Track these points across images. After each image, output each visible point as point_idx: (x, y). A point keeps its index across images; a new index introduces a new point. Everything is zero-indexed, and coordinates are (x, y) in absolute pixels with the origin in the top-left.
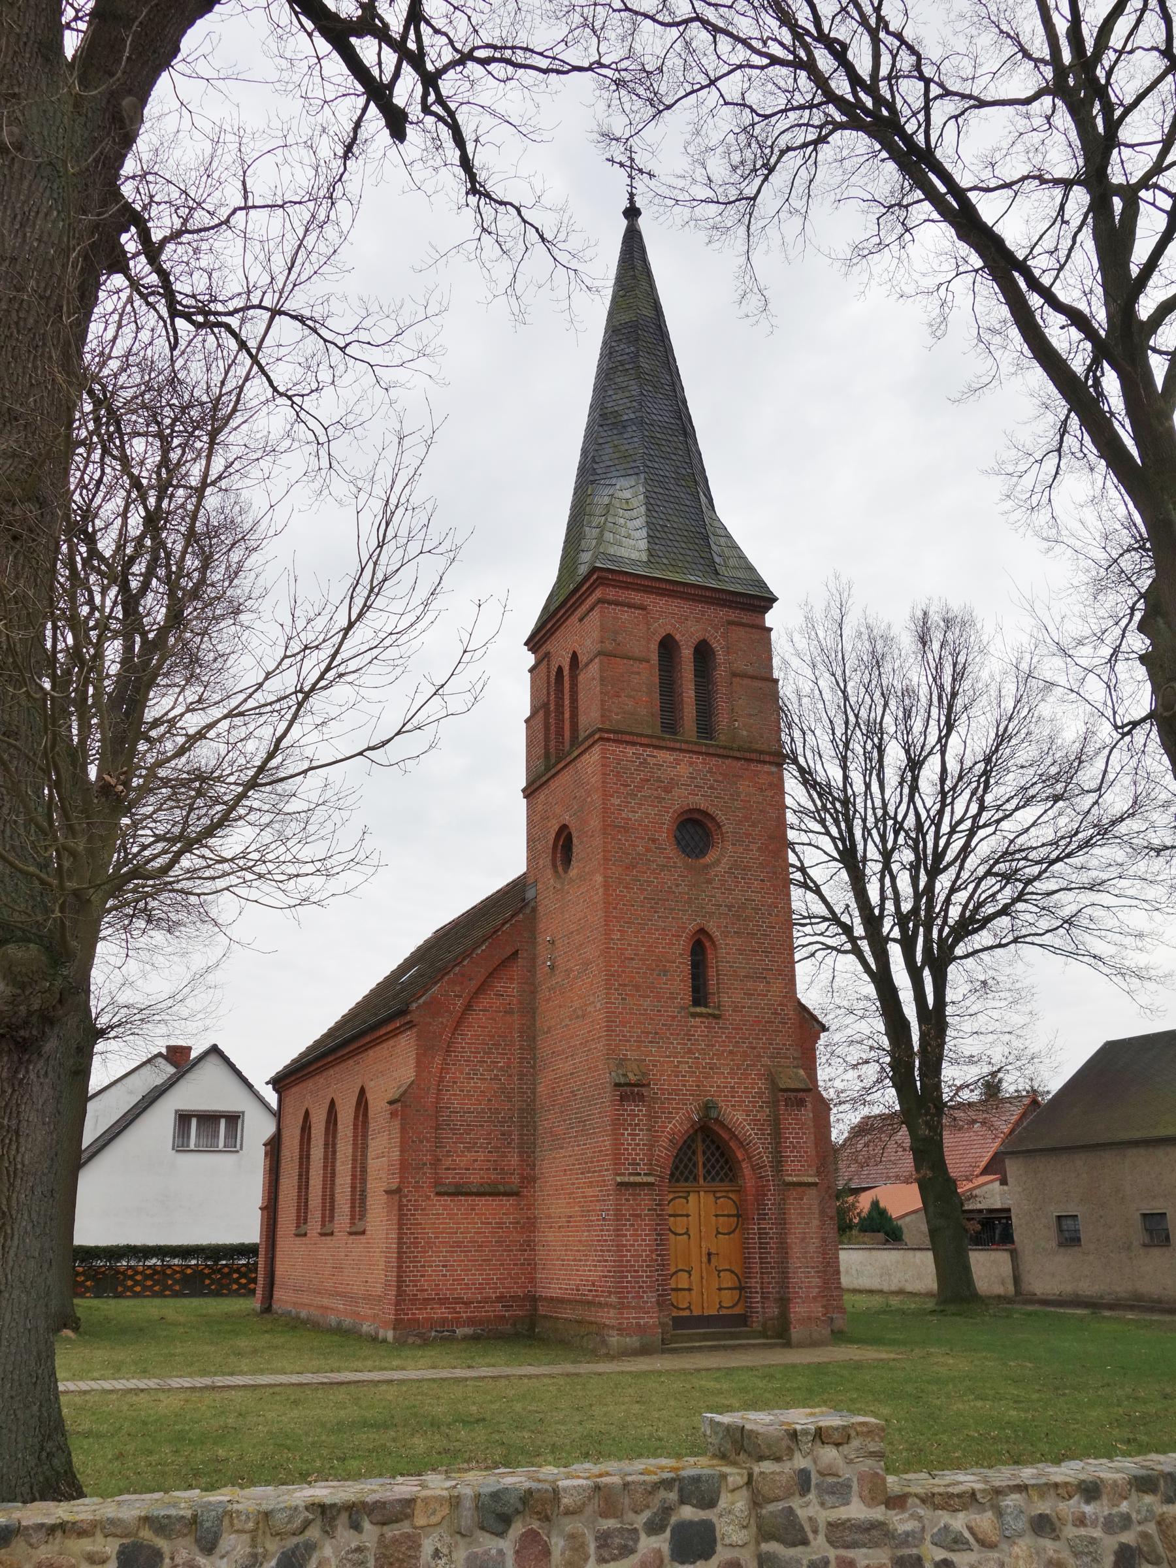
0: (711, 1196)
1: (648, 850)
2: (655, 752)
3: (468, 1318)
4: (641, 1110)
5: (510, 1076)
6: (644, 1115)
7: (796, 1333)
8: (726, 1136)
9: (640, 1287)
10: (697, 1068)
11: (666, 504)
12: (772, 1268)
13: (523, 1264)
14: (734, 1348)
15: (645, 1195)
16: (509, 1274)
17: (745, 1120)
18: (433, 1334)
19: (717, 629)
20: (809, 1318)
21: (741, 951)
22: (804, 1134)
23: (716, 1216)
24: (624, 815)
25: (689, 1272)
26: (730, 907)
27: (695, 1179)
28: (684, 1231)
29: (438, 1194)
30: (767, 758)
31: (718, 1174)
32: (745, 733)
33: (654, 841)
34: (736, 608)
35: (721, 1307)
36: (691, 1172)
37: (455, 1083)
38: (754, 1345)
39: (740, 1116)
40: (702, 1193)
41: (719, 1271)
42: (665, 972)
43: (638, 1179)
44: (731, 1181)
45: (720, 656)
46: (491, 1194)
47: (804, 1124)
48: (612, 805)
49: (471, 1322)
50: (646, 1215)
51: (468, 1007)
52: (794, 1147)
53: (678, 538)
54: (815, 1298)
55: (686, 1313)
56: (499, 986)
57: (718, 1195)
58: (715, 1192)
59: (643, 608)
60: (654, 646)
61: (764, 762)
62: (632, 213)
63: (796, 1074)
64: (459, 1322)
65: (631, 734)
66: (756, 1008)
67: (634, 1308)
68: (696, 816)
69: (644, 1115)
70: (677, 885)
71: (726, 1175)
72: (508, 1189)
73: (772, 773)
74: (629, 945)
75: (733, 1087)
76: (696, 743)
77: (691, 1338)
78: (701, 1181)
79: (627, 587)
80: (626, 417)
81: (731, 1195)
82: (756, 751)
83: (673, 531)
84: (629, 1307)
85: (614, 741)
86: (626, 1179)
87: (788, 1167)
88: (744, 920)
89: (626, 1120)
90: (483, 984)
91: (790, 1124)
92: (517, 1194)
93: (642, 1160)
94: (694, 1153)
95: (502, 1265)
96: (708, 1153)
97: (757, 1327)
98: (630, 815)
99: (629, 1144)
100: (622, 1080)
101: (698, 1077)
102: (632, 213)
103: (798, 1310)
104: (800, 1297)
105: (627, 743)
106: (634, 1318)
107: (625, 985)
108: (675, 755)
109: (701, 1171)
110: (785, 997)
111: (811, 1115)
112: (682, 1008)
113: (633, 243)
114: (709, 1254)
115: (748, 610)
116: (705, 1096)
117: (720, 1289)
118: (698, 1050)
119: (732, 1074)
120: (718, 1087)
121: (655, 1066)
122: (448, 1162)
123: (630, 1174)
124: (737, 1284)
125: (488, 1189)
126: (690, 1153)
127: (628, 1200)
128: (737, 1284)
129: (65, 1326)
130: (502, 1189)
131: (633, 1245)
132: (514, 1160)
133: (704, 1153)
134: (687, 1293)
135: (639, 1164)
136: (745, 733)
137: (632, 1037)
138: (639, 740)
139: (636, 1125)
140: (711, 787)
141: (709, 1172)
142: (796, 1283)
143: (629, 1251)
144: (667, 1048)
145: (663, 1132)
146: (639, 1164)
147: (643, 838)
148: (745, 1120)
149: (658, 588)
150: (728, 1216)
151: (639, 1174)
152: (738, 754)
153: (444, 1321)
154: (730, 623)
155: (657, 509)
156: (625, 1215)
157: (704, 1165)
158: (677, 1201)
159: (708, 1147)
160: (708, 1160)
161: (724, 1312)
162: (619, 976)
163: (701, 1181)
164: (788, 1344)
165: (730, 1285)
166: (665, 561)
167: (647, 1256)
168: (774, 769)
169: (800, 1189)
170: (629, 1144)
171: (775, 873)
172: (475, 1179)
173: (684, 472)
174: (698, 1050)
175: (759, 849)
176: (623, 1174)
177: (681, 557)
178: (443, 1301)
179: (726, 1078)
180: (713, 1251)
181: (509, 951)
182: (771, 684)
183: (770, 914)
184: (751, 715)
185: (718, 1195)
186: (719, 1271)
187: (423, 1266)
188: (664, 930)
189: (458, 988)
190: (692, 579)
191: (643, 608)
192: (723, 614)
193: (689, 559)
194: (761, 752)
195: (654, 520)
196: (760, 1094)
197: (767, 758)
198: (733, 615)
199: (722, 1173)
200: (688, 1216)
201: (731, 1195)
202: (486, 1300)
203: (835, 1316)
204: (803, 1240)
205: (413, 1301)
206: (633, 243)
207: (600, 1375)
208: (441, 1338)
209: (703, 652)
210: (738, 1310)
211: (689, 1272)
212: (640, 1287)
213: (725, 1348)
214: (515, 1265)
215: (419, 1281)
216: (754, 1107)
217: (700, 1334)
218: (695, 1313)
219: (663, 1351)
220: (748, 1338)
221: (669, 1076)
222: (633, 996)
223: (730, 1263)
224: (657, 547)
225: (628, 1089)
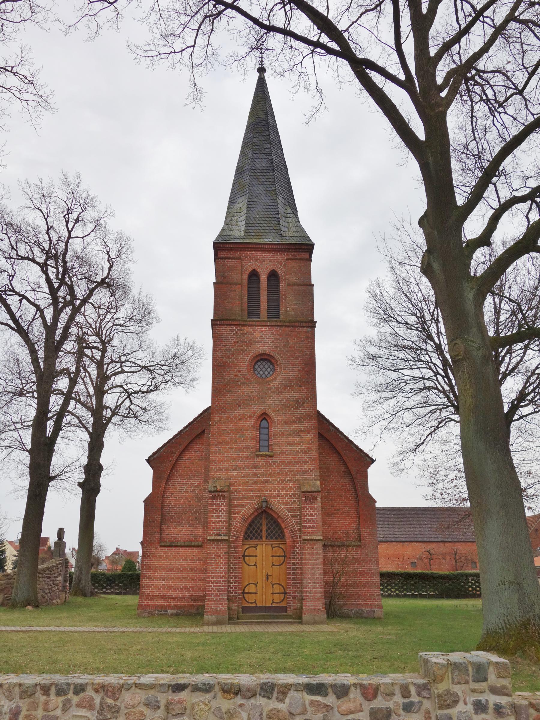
1: (236, 376)
2: (242, 328)
3: (174, 605)
4: (223, 504)
5: (200, 490)
7: (305, 617)
9: (218, 591)
10: (259, 482)
11: (257, 206)
12: (297, 583)
13: (202, 580)
14: (270, 623)
15: (223, 545)
16: (196, 585)
18: (157, 612)
19: (281, 263)
20: (314, 609)
21: (286, 423)
23: (272, 556)
24: (224, 360)
25: (256, 585)
26: (281, 401)
27: (261, 538)
28: (254, 564)
29: (161, 546)
30: (305, 324)
31: (274, 535)
32: (293, 313)
33: (239, 371)
34: (292, 252)
35: (273, 602)
36: (259, 534)
37: (173, 494)
38: (282, 623)
39: (282, 506)
40: (264, 545)
41: (273, 585)
42: (243, 435)
43: (220, 538)
44: (281, 539)
45: (282, 277)
46: (187, 546)
48: (218, 356)
49: (175, 607)
50: (223, 556)
51: (179, 457)
52: (310, 521)
53: (262, 222)
54: (318, 599)
55: (254, 605)
56: (196, 447)
57: (274, 546)
58: (272, 544)
59: (239, 258)
60: (245, 277)
61: (303, 327)
62: (261, 70)
63: (314, 483)
64: (169, 607)
65: (228, 320)
66: (294, 451)
67: (214, 601)
68: (265, 357)
69: (224, 506)
70: (251, 392)
71: (279, 535)
72: (196, 544)
73: (308, 332)
74: (224, 423)
75: (279, 491)
76: (267, 321)
77: (251, 618)
78: (264, 539)
79: (231, 249)
80: (245, 168)
81: (281, 546)
82: (298, 321)
83: (260, 219)
84: (211, 601)
85: (220, 325)
87: (306, 531)
88: (289, 407)
89: (215, 509)
90: (186, 447)
91: (308, 509)
92: (201, 546)
93: (223, 528)
94: (261, 525)
95: (193, 580)
96: (269, 525)
97: (289, 613)
98: (227, 360)
102: (261, 70)
103: (308, 604)
104: (310, 598)
105: (227, 325)
106: (214, 606)
107: (221, 443)
108: (253, 328)
109: (264, 534)
110: (311, 444)
112: (252, 453)
113: (261, 85)
114: (268, 576)
115: (299, 252)
117: (273, 593)
118: (260, 473)
119: (278, 484)
120: (270, 491)
122: (168, 531)
123: (215, 535)
124: (283, 591)
125: (186, 544)
127: (214, 548)
128: (283, 591)
129: (29, 605)
130: (193, 544)
131: (216, 571)
132: (201, 530)
133: (267, 525)
136: (293, 313)
137: (223, 468)
138: (233, 323)
139: (220, 511)
140: (273, 342)
141: (269, 534)
143: (213, 573)
144: (242, 473)
145: (238, 514)
147: (234, 370)
149: (248, 248)
150: (279, 556)
151: (220, 535)
152: (288, 324)
153: (162, 606)
154: (288, 259)
155: (252, 209)
157: (267, 531)
158: (250, 549)
159: (269, 522)
160: (269, 528)
162: (217, 439)
163: (264, 539)
164: (301, 623)
165: (278, 591)
166: (253, 234)
168: (309, 329)
169: (311, 542)
170: (215, 521)
171: (307, 382)
172: (181, 539)
173: (270, 189)
174: (260, 473)
175: (299, 371)
176: (212, 535)
177: (262, 231)
178: (162, 597)
180: (270, 574)
181: (200, 431)
182: (309, 287)
183: (304, 403)
184: (297, 304)
185: (274, 546)
186: (273, 585)
187: (153, 580)
188: (243, 414)
189: (173, 450)
190: (267, 241)
191: (239, 258)
192: (285, 255)
193: (267, 231)
194: (301, 322)
195: (250, 215)
196: (294, 494)
197: (305, 324)
198: (290, 255)
199: (277, 535)
200: (256, 556)
201: (281, 546)
202: (184, 597)
203: (376, 610)
204: (312, 569)
205: (148, 596)
206: (261, 85)
208: (160, 614)
209: (273, 276)
210: (283, 604)
211: (256, 585)
212: (218, 591)
213: (265, 623)
214: (199, 580)
215: (151, 587)
217: (256, 616)
218: (258, 605)
220: (278, 619)
222: (225, 448)
223: (279, 581)
224: (250, 228)
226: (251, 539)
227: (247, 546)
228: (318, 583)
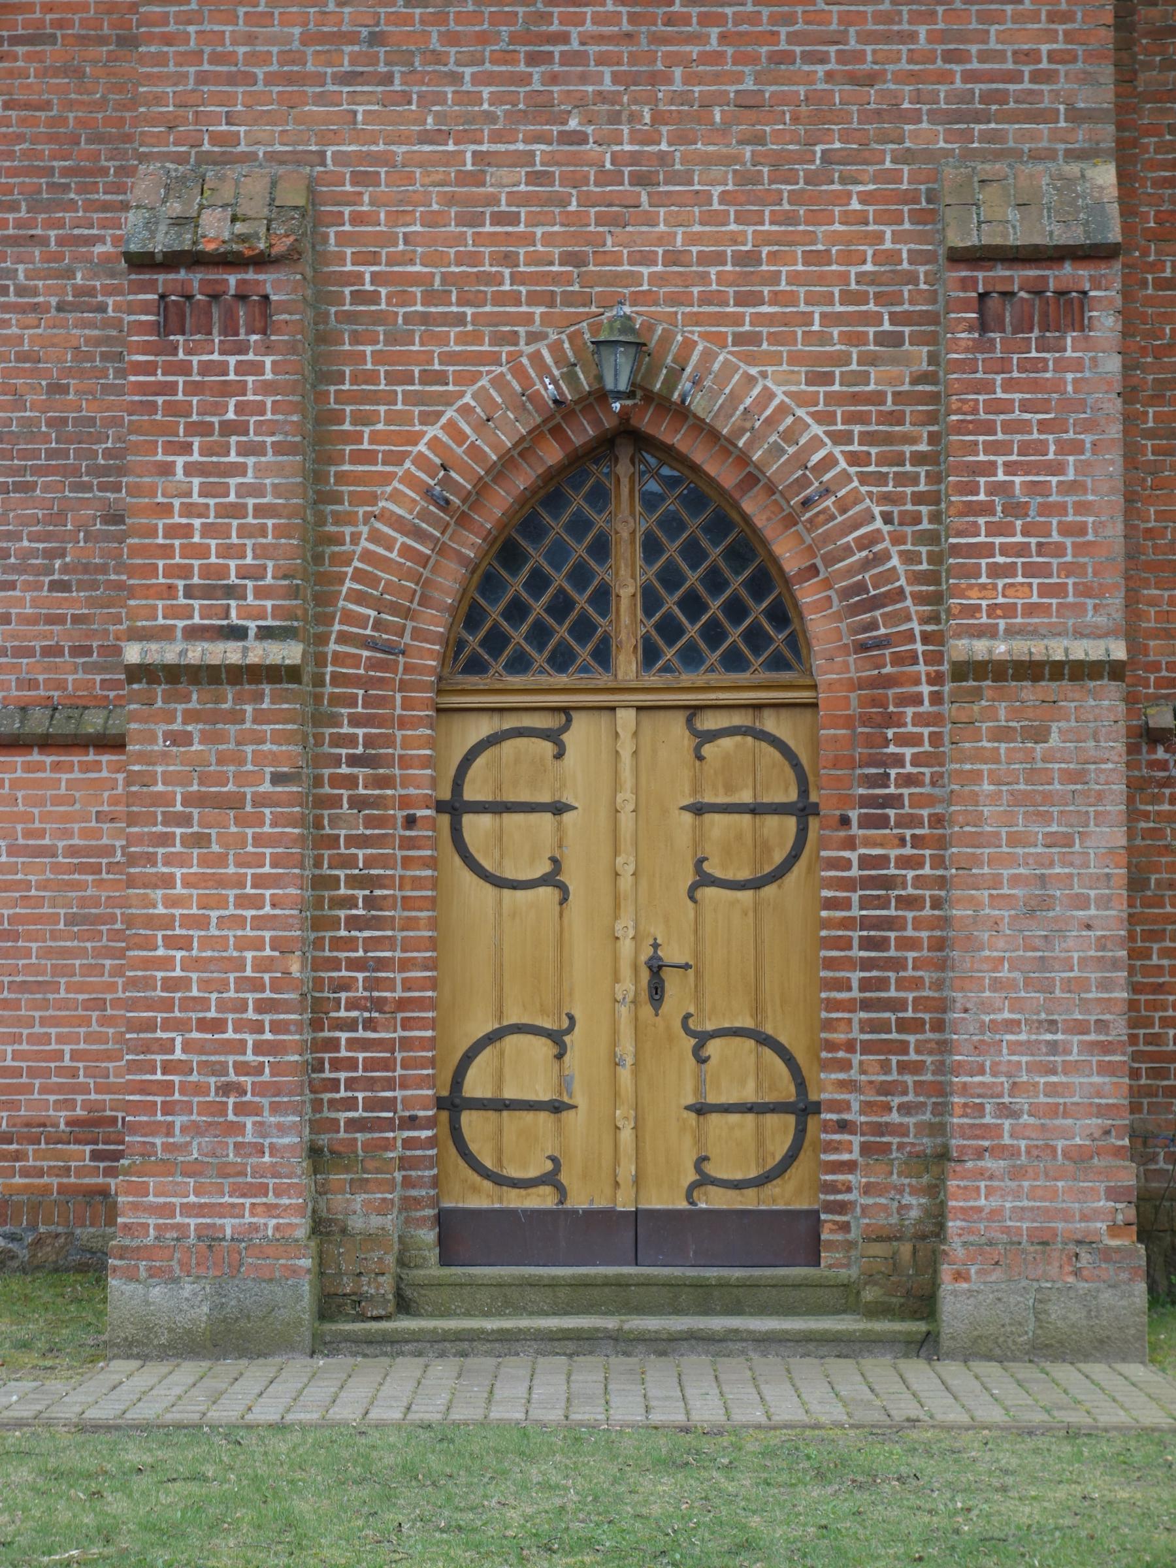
0: (676, 725)
6: (267, 388)
8: (724, 474)
9: (226, 1089)
10: (577, 181)
17: (803, 400)
22: (1065, 448)
23: (698, 810)
25: (557, 1038)
27: (603, 656)
35: (705, 1180)
38: (764, 1341)
40: (627, 718)
41: (703, 1038)
43: (230, 653)
44: (778, 663)
46: (46, 743)
47: (1068, 405)
50: (261, 801)
52: (1015, 509)
54: (1080, 1158)
55: (541, 1199)
58: (694, 711)
69: (267, 388)
78: (627, 665)
81: (770, 723)
84: (167, 1167)
86: (169, 653)
89: (183, 410)
91: (1003, 407)
93: (255, 573)
94: (601, 549)
96: (672, 549)
99: (189, 510)
100: (162, 242)
101: (578, 219)
106: (187, 1209)
111: (1113, 364)
114: (656, 968)
116: (607, 302)
117: (701, 1110)
118: (581, 103)
120: (673, 258)
121: (370, 179)
123: (192, 634)
125: (38, 723)
126: (580, 550)
128: (786, 1090)
131: (201, 922)
133: (652, 548)
134: (543, 1119)
135: (231, 592)
137: (254, 58)
139: (229, 428)
141: (669, 630)
142: (990, 1091)
143: (184, 943)
145: (399, 459)
146: (231, 592)
148: (803, 400)
151: (238, 633)
156: (165, 800)
157: (650, 601)
160: (670, 578)
161: (715, 1200)
163: (627, 665)
165: (748, 1093)
167: (262, 965)
169: (1028, 692)
170: (189, 510)
174: (581, 103)
176: (165, 634)
179: (720, 219)
180: (673, 953)
185: (710, 722)
186: (703, 1038)
200: (558, 809)
201: (770, 723)
207: (656, 1428)
211: (557, 1038)
212: (226, 1089)
216: (858, 339)
217: (553, 1284)
218: (578, 1201)
219: (320, 1346)
220: (736, 1309)
221: (431, 220)
225: (195, 279)
226: (519, 664)
227: (483, 727)
228: (1080, 1028)
